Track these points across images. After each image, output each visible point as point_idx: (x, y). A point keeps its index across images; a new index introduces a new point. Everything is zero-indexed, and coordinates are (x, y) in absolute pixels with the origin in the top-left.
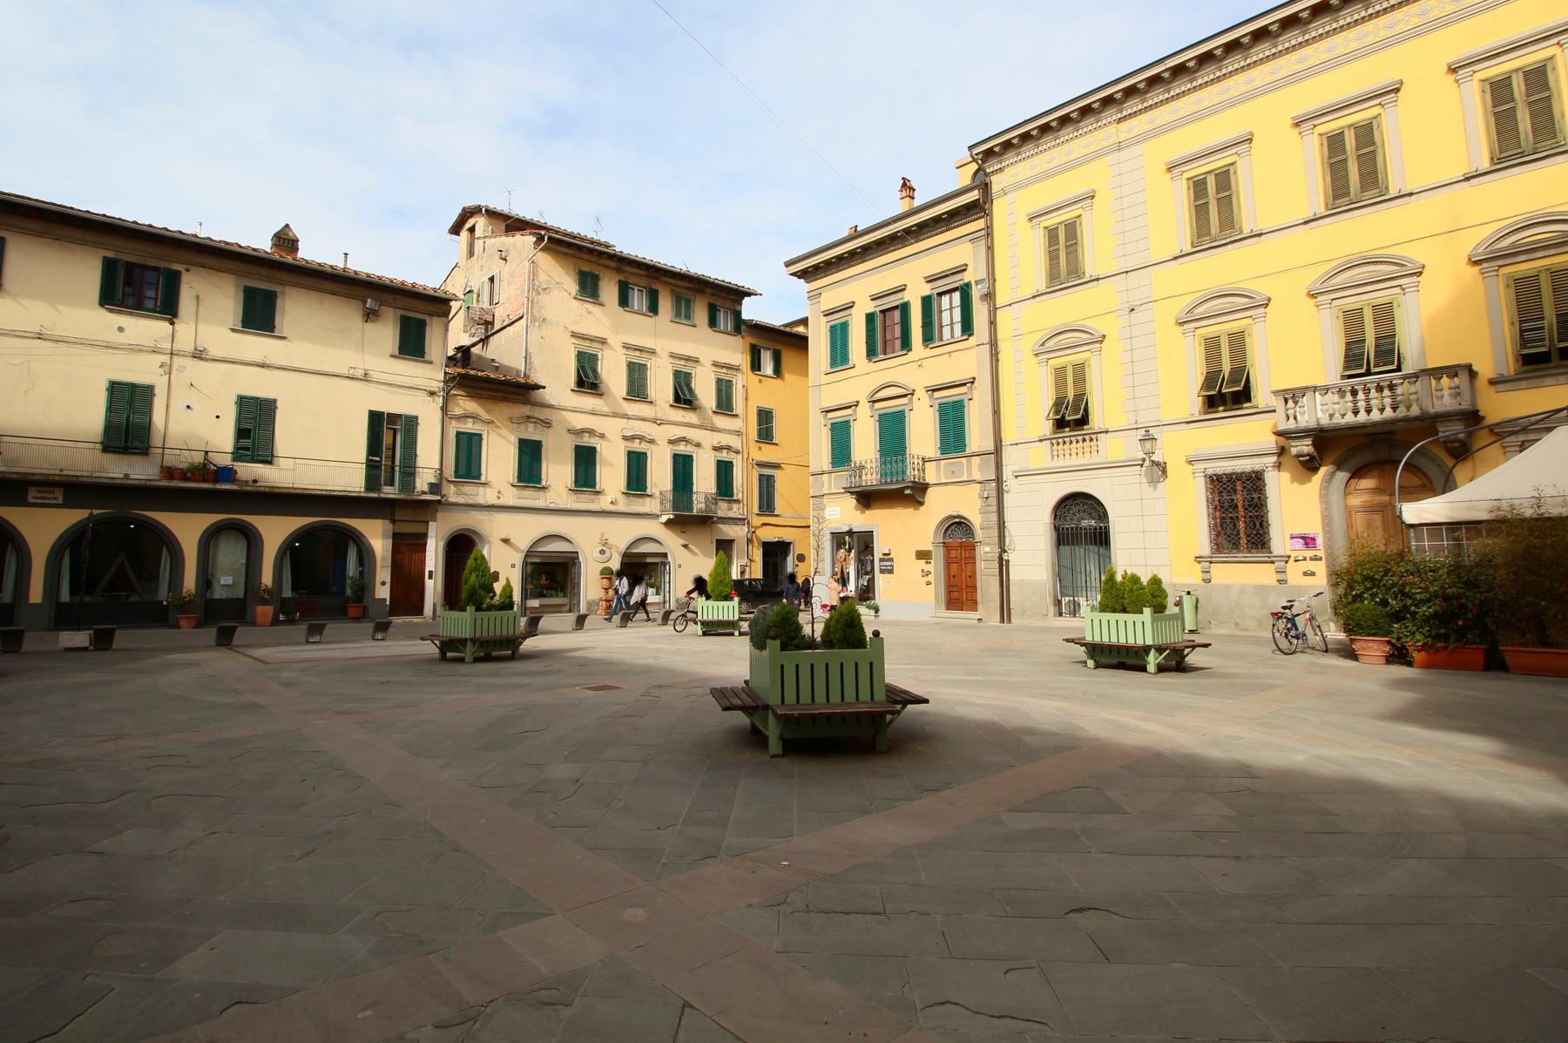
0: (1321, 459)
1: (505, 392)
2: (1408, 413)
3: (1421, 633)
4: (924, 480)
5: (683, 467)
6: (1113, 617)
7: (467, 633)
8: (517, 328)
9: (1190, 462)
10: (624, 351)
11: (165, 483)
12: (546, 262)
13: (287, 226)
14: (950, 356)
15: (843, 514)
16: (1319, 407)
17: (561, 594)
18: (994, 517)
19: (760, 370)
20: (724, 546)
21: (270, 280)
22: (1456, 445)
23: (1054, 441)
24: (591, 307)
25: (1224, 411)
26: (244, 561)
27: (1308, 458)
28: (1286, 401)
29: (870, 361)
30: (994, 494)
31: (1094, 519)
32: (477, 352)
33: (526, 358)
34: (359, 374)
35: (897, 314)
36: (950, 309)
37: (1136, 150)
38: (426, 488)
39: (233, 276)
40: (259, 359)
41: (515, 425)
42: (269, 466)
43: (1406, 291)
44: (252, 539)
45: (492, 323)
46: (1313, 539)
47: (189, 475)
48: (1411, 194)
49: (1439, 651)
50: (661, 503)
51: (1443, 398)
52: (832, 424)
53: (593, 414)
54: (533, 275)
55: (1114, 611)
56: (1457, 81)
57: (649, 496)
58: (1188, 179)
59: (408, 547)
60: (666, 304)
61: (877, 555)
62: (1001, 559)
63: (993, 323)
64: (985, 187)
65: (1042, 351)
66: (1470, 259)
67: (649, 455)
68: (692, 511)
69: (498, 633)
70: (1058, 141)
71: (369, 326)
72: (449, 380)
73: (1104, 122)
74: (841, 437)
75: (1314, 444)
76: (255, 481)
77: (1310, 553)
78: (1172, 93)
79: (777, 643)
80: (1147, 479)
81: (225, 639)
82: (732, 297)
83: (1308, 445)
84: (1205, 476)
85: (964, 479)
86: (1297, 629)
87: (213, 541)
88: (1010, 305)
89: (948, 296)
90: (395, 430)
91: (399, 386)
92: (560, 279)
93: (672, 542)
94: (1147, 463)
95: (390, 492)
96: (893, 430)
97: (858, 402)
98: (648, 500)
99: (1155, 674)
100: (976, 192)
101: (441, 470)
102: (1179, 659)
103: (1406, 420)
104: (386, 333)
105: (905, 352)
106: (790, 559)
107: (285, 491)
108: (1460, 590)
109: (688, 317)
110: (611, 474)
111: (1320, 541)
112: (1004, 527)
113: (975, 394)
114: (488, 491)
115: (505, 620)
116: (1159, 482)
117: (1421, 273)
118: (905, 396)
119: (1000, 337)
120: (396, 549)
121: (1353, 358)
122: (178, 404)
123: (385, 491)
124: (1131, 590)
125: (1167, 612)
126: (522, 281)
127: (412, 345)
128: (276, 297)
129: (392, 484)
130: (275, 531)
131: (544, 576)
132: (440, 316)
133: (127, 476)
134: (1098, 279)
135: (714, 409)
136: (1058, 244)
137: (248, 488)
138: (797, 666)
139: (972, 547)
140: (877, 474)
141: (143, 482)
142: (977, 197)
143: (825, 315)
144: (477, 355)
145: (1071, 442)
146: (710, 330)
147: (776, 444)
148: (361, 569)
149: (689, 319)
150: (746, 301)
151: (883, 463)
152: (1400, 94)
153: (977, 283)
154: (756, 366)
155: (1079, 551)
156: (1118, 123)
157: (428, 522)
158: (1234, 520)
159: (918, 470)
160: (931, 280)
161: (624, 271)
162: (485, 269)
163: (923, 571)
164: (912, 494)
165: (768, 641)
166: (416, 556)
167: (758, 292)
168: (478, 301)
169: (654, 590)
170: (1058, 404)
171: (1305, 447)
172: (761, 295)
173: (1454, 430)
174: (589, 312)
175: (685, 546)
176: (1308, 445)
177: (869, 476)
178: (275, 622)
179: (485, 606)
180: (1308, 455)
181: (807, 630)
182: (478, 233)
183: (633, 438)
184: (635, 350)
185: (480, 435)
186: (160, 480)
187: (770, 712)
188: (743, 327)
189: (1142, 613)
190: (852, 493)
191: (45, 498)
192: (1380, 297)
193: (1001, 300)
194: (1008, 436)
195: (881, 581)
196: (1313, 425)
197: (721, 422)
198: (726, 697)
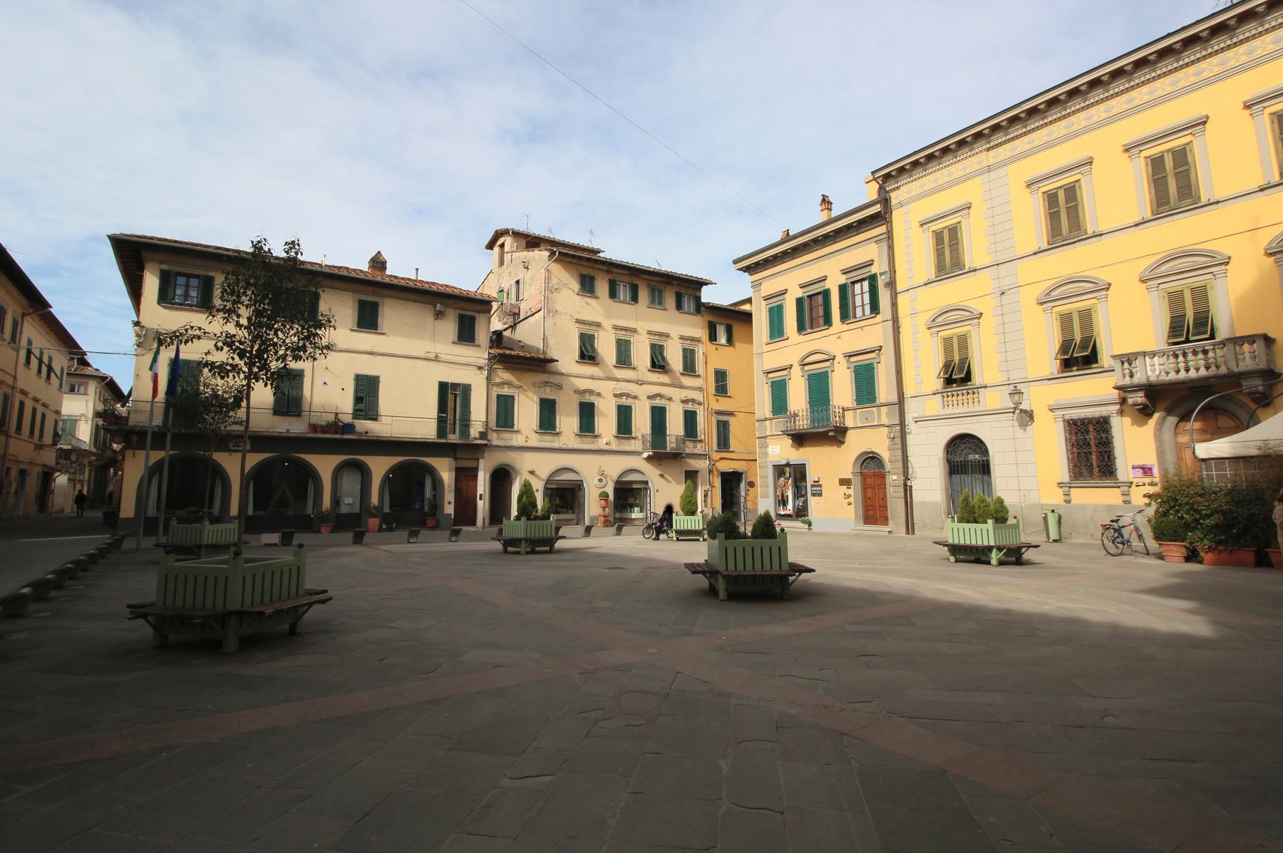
0: (1154, 408)
1: (529, 365)
2: (1218, 372)
3: (1208, 539)
4: (844, 425)
5: (658, 415)
7: (521, 534)
8: (537, 318)
9: (1051, 410)
10: (614, 331)
12: (557, 269)
13: (379, 252)
15: (781, 451)
16: (1149, 368)
17: (570, 511)
18: (899, 453)
19: (716, 341)
20: (691, 475)
21: (374, 294)
22: (1257, 396)
23: (945, 394)
24: (589, 300)
25: (1077, 370)
26: (359, 487)
27: (1141, 406)
28: (1123, 363)
29: (800, 334)
30: (898, 435)
32: (508, 335)
33: (543, 339)
36: (861, 294)
38: (477, 436)
39: (351, 294)
40: (368, 349)
41: (537, 389)
42: (375, 422)
43: (1217, 276)
44: (364, 471)
45: (518, 314)
46: (1150, 469)
47: (326, 429)
48: (1218, 202)
49: (1221, 552)
50: (643, 444)
51: (1249, 359)
53: (592, 378)
54: (548, 279)
55: (968, 522)
56: (1251, 115)
57: (633, 438)
58: (1043, 193)
59: (466, 476)
60: (643, 295)
61: (809, 482)
62: (905, 485)
63: (894, 305)
64: (884, 200)
65: (933, 325)
66: (1266, 252)
67: (633, 408)
68: (666, 450)
69: (541, 535)
70: (941, 166)
71: (438, 322)
72: (492, 358)
73: (977, 150)
74: (779, 392)
75: (1147, 396)
76: (366, 433)
77: (1147, 480)
78: (1028, 128)
79: (723, 535)
80: (1019, 423)
81: (358, 539)
82: (694, 286)
83: (1141, 397)
84: (1064, 421)
85: (875, 423)
86: (1123, 537)
87: (339, 474)
88: (908, 290)
89: (859, 284)
90: (456, 395)
91: (458, 364)
92: (567, 281)
93: (652, 473)
94: (1017, 412)
95: (453, 438)
96: (819, 387)
97: (792, 365)
98: (633, 441)
99: (996, 566)
100: (878, 206)
101: (487, 422)
102: (1018, 556)
103: (1216, 377)
104: (449, 327)
106: (743, 485)
107: (387, 439)
108: (1232, 508)
109: (660, 303)
110: (606, 424)
111: (1156, 471)
112: (907, 461)
113: (883, 359)
114: (519, 436)
115: (545, 527)
116: (1027, 425)
117: (1228, 263)
118: (828, 360)
119: (901, 314)
120: (458, 480)
121: (1177, 329)
123: (450, 438)
124: (979, 507)
126: (540, 284)
127: (466, 334)
128: (378, 306)
129: (454, 433)
130: (379, 466)
131: (558, 498)
133: (288, 430)
134: (975, 270)
136: (944, 244)
137: (363, 438)
138: (735, 548)
139: (882, 476)
140: (807, 420)
141: (299, 435)
142: (880, 210)
143: (765, 300)
144: (507, 337)
145: (958, 395)
146: (677, 312)
147: (730, 397)
148: (434, 493)
149: (661, 304)
150: (704, 288)
151: (812, 412)
152: (1206, 126)
153: (881, 274)
154: (713, 337)
155: (967, 478)
156: (987, 151)
157: (478, 459)
158: (1088, 455)
159: (839, 417)
160: (845, 272)
161: (613, 273)
162: (513, 275)
163: (845, 494)
164: (836, 436)
165: (718, 534)
166: (471, 483)
167: (714, 282)
168: (508, 298)
169: (639, 509)
170: (947, 366)
171: (1139, 398)
172: (715, 284)
173: (1258, 385)
174: (588, 304)
175: (662, 476)
176: (1141, 397)
177: (801, 422)
178: (381, 530)
179: (532, 517)
180: (1142, 404)
181: (742, 529)
182: (507, 248)
183: (620, 396)
184: (622, 330)
185: (513, 397)
186: (308, 433)
190: (788, 435)
192: (1196, 281)
193: (900, 287)
194: (909, 390)
195: (813, 502)
196: (1143, 381)
197: (687, 381)
198: (694, 569)
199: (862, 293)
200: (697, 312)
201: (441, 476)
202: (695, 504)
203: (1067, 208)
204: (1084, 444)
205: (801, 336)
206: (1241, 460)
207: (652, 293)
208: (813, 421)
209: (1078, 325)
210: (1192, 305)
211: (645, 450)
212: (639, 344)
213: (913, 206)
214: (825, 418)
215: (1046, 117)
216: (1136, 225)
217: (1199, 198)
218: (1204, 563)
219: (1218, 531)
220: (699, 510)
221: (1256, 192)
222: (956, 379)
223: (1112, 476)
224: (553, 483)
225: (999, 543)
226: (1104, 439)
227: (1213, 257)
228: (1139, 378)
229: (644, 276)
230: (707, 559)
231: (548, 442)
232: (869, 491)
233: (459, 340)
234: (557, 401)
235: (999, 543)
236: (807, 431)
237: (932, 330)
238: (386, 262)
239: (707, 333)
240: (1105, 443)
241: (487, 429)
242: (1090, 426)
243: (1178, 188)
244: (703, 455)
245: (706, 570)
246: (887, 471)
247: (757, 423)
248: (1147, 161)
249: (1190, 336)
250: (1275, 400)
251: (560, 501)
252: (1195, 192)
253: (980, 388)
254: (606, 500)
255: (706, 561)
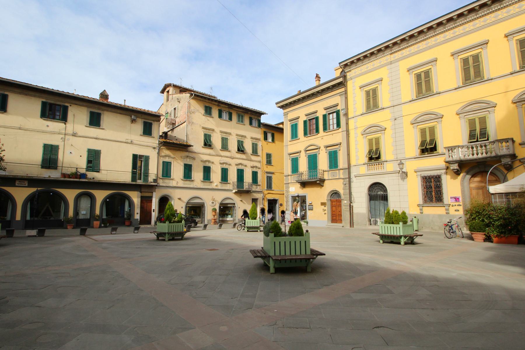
0: (461, 171)
1: (179, 148)
3: (496, 231)
4: (324, 178)
5: (240, 174)
6: (389, 225)
7: (166, 230)
9: (415, 172)
10: (220, 133)
11: (63, 179)
12: (194, 103)
13: (105, 90)
14: (332, 135)
15: (295, 190)
17: (198, 217)
18: (348, 191)
19: (267, 140)
20: (255, 201)
21: (99, 109)
22: (508, 166)
24: (209, 118)
25: (428, 154)
26: (90, 206)
27: (456, 170)
28: (449, 151)
29: (305, 137)
30: (348, 183)
31: (382, 191)
32: (170, 134)
33: (186, 136)
34: (129, 141)
35: (314, 121)
36: (332, 119)
37: (397, 64)
38: (152, 181)
39: (86, 108)
40: (95, 136)
41: (183, 159)
42: (98, 173)
43: (490, 112)
44: (92, 198)
45: (175, 124)
46: (458, 199)
48: (492, 79)
49: (502, 237)
50: (233, 186)
51: (503, 150)
52: (292, 159)
53: (210, 155)
54: (189, 107)
55: (389, 223)
58: (415, 74)
59: (146, 201)
60: (235, 117)
61: (308, 204)
62: (350, 205)
63: (347, 124)
65: (364, 133)
66: (512, 102)
69: (177, 231)
70: (370, 61)
71: (133, 125)
73: (386, 54)
74: (295, 163)
75: (459, 166)
76: (93, 178)
77: (457, 203)
78: (409, 44)
79: (273, 234)
80: (401, 178)
81: (83, 233)
82: (258, 115)
83: (456, 166)
84: (421, 177)
86: (453, 230)
87: (79, 199)
88: (353, 117)
89: (332, 115)
90: (142, 161)
91: (143, 146)
92: (198, 108)
93: (236, 199)
94: (401, 172)
95: (140, 182)
96: (313, 161)
99: (404, 245)
100: (342, 79)
101: (157, 174)
102: (412, 240)
104: (139, 127)
105: (317, 134)
106: (277, 205)
107: (104, 181)
108: (509, 216)
109: (242, 122)
110: (216, 176)
111: (461, 199)
112: (351, 194)
113: (341, 148)
115: (179, 226)
117: (495, 106)
118: (317, 149)
119: (350, 128)
121: (472, 136)
122: (67, 152)
123: (138, 182)
124: (395, 216)
125: (408, 224)
126: (185, 110)
127: (147, 131)
129: (140, 179)
130: (100, 195)
131: (193, 211)
132: (157, 122)
134: (384, 109)
135: (251, 153)
137: (91, 181)
140: (307, 176)
141: (55, 179)
142: (342, 80)
143: (289, 121)
144: (170, 135)
145: (374, 165)
147: (272, 166)
148: (130, 208)
149: (243, 122)
150: (262, 116)
151: (310, 172)
152: (488, 45)
153: (342, 110)
154: (266, 138)
155: (377, 202)
156: (390, 55)
157: (153, 192)
158: (431, 192)
160: (326, 109)
163: (323, 209)
164: (320, 183)
167: (267, 113)
168: (170, 116)
169: (231, 216)
171: (455, 166)
172: (267, 114)
173: (507, 161)
174: (208, 120)
175: (241, 201)
176: (456, 166)
177: (305, 177)
178: (100, 227)
179: (172, 221)
180: (457, 169)
181: (283, 230)
182: (170, 93)
183: (223, 163)
184: (224, 133)
186: (61, 178)
187: (271, 258)
188: (261, 125)
189: (399, 224)
190: (299, 182)
191: (21, 184)
192: (481, 115)
193: (350, 116)
194: (353, 162)
195: (309, 213)
196: (458, 159)
197: (254, 158)
198: (255, 253)
199: (333, 119)
200: (258, 127)
201: (133, 200)
202: (256, 214)
203: (425, 81)
204: (429, 187)
205: (305, 138)
206: (510, 194)
207: (238, 117)
208: (310, 176)
209: (429, 135)
210: (479, 125)
211: (234, 189)
212: (232, 140)
213: (357, 79)
214: (315, 175)
215: (417, 40)
216: (456, 89)
217: (484, 77)
218: (494, 242)
219: (501, 228)
220: (258, 217)
221: (509, 75)
222: (374, 158)
223: (442, 202)
224: (190, 204)
225: (405, 234)
226: (438, 185)
227: (487, 103)
228: (456, 158)
229: (235, 109)
230: (263, 246)
231: (188, 184)
232: (334, 208)
233: (143, 134)
234: (192, 165)
235: (405, 234)
236: (308, 181)
237: (364, 136)
238: (108, 96)
239: (263, 136)
240: (439, 187)
241: (157, 178)
242: (432, 179)
243: (475, 73)
244: (260, 191)
245: (262, 254)
246: (342, 199)
247: (285, 177)
248: (461, 60)
249: (479, 139)
250: (514, 169)
251: (193, 212)
252: (482, 74)
253: (385, 162)
254: (215, 212)
255: (262, 248)
